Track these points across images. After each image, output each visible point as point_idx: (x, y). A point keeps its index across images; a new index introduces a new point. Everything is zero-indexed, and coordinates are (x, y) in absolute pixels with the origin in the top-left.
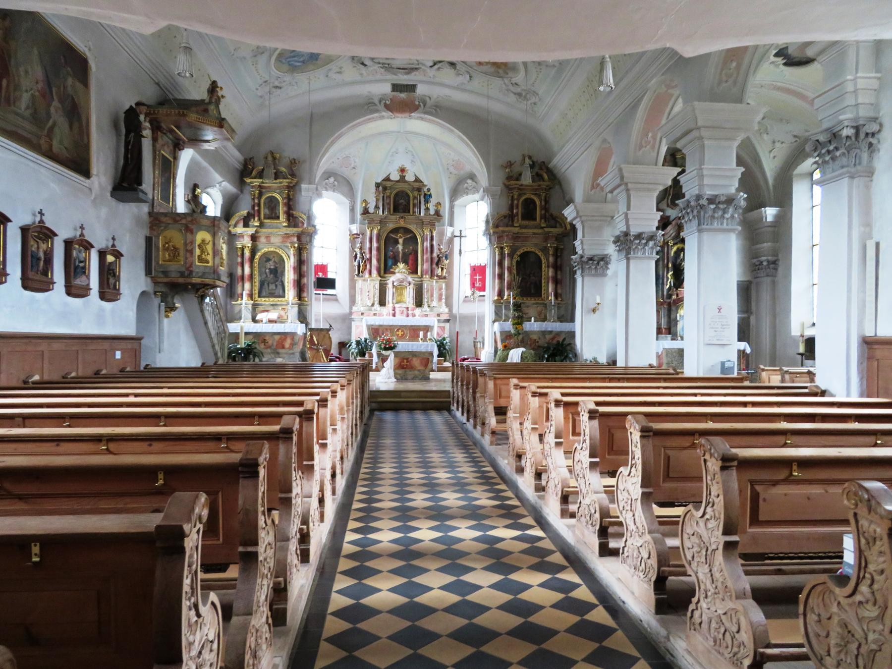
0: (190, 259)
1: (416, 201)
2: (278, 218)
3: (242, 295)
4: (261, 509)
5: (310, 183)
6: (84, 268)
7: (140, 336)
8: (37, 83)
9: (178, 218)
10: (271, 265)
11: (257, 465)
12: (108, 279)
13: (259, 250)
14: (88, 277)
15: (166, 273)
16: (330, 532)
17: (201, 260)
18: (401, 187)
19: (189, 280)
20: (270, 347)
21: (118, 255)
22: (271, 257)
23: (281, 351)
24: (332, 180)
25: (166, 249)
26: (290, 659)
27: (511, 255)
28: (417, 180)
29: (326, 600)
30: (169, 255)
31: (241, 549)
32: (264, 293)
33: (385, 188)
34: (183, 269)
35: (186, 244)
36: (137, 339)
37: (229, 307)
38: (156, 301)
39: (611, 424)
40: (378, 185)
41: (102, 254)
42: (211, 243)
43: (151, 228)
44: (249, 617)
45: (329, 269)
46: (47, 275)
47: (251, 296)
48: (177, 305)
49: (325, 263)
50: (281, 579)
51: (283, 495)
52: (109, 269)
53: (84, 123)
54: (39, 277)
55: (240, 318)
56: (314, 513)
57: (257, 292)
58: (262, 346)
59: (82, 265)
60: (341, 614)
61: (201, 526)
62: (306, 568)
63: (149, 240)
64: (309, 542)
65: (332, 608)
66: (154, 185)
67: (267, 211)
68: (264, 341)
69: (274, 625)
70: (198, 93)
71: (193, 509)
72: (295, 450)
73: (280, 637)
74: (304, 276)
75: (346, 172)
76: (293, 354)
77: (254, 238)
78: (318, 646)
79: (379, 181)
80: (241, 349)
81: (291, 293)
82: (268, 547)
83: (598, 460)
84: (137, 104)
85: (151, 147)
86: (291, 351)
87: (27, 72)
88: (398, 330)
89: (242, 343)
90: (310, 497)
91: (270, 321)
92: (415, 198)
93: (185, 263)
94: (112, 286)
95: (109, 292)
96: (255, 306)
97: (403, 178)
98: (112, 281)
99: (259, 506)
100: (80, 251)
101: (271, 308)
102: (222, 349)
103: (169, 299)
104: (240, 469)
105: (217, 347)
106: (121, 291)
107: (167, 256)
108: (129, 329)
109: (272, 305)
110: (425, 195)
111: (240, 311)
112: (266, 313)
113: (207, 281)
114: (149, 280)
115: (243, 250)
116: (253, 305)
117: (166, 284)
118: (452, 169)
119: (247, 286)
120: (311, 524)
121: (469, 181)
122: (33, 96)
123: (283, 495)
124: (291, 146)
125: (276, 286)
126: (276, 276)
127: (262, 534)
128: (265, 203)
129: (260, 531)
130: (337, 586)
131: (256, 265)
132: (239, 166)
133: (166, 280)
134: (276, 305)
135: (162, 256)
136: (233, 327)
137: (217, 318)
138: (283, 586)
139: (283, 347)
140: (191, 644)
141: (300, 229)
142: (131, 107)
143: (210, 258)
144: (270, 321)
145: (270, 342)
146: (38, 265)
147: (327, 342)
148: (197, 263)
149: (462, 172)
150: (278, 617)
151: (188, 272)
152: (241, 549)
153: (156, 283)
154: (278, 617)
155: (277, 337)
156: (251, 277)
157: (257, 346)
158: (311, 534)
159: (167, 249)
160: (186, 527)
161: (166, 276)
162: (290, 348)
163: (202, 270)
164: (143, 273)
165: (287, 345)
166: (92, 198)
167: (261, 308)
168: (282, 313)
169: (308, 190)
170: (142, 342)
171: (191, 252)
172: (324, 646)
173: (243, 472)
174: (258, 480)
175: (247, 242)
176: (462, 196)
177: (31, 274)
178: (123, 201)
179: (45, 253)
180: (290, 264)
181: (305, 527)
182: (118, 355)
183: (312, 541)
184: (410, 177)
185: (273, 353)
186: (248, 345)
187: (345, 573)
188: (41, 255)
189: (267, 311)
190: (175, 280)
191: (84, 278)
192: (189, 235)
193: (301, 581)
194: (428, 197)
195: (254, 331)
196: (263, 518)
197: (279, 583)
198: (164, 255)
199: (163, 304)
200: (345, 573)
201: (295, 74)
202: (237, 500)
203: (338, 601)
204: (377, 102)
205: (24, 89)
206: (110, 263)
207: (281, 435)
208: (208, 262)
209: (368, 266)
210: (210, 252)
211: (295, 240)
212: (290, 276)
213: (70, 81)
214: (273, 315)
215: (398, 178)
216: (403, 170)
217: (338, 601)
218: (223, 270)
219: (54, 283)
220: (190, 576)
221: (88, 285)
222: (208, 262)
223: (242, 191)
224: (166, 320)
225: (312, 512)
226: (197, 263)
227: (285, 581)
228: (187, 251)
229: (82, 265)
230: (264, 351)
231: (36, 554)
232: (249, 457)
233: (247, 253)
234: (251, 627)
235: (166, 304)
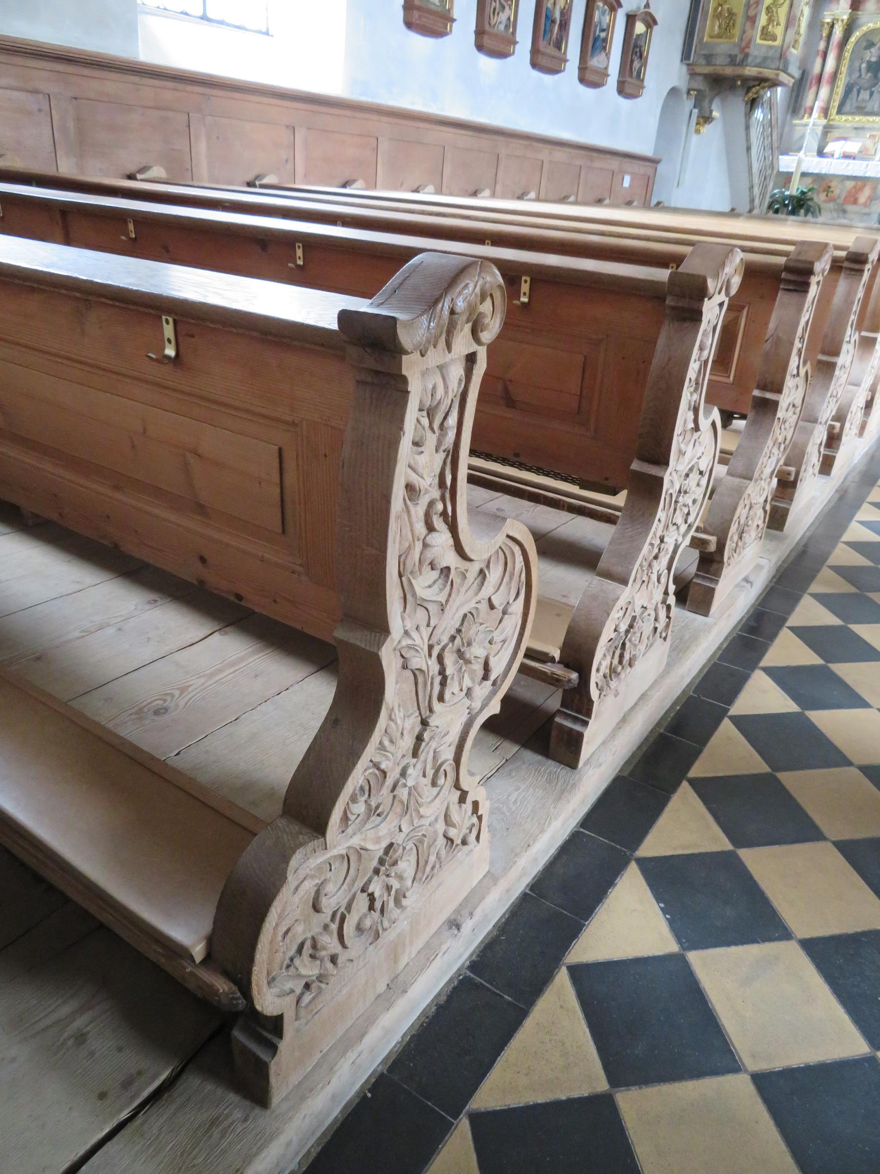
0: (749, 33)
3: (812, 109)
4: (797, 344)
6: (605, 40)
7: (657, 157)
11: (810, 272)
12: (632, 62)
13: (860, 26)
14: (608, 55)
16: (866, 454)
17: (766, 34)
19: (739, 71)
20: (833, 200)
21: (651, 22)
22: (876, 40)
23: (850, 208)
25: (718, 16)
26: (777, 570)
29: (843, 527)
30: (720, 27)
31: (756, 393)
32: (847, 107)
34: (736, 51)
36: (653, 162)
37: (786, 129)
41: (631, 19)
44: (748, 482)
46: (559, 48)
47: (825, 112)
48: (715, 114)
50: (792, 469)
51: (824, 358)
52: (636, 46)
54: (551, 50)
55: (799, 150)
56: (855, 416)
57: (836, 104)
58: (823, 196)
59: (603, 35)
60: (753, 727)
61: (727, 300)
62: (824, 481)
64: (838, 448)
65: (847, 537)
68: (828, 189)
69: (768, 527)
71: (723, 265)
72: (860, 294)
73: (771, 540)
76: (868, 214)
78: (818, 571)
80: (791, 197)
82: (791, 409)
86: (866, 210)
89: (794, 189)
90: (858, 385)
91: (846, 156)
93: (741, 39)
94: (635, 74)
95: (630, 84)
96: (827, 130)
98: (636, 65)
99: (797, 340)
100: (603, 13)
101: (853, 134)
102: (763, 194)
103: (706, 103)
104: (783, 275)
105: (756, 191)
106: (646, 83)
107: (716, 28)
108: (643, 145)
109: (856, 129)
111: (802, 137)
112: (843, 142)
113: (767, 73)
114: (684, 68)
115: (832, 26)
116: (825, 127)
117: (706, 77)
119: (824, 91)
120: (847, 425)
123: (824, 358)
125: (872, 94)
127: (789, 382)
129: (788, 377)
130: (860, 516)
131: (847, 55)
133: (707, 70)
134: (863, 128)
135: (710, 27)
136: (786, 163)
137: (766, 143)
138: (792, 478)
139: (855, 202)
140: (681, 453)
143: (779, 31)
144: (846, 156)
145: (837, 192)
146: (551, 31)
148: (759, 41)
150: (777, 519)
151: (739, 59)
152: (756, 393)
153: (693, 75)
154: (777, 519)
155: (850, 184)
157: (815, 197)
158: (844, 438)
160: (711, 284)
161: (709, 64)
162: (865, 205)
164: (678, 56)
165: (863, 198)
167: (836, 133)
168: (869, 143)
170: (660, 167)
172: (826, 573)
173: (789, 282)
174: (806, 297)
177: (542, 44)
179: (562, 14)
181: (838, 425)
182: (627, 181)
183: (842, 448)
186: (803, 193)
187: (802, 633)
188: (557, 15)
190: (719, 70)
191: (603, 56)
193: (813, 495)
195: (816, 171)
196: (797, 359)
197: (789, 474)
198: (713, 26)
199: (696, 111)
200: (802, 633)
202: (767, 324)
203: (761, 696)
206: (639, 36)
207: (846, 264)
208: (774, 38)
210: (783, 19)
214: (852, 147)
217: (761, 696)
218: (795, 53)
219: (566, 61)
220: (698, 364)
221: (606, 68)
222: (774, 38)
224: (694, 138)
225: (853, 408)
226: (759, 41)
227: (797, 474)
229: (603, 35)
230: (823, 206)
231: (525, 294)
232: (802, 258)
234: (745, 496)
235: (700, 111)
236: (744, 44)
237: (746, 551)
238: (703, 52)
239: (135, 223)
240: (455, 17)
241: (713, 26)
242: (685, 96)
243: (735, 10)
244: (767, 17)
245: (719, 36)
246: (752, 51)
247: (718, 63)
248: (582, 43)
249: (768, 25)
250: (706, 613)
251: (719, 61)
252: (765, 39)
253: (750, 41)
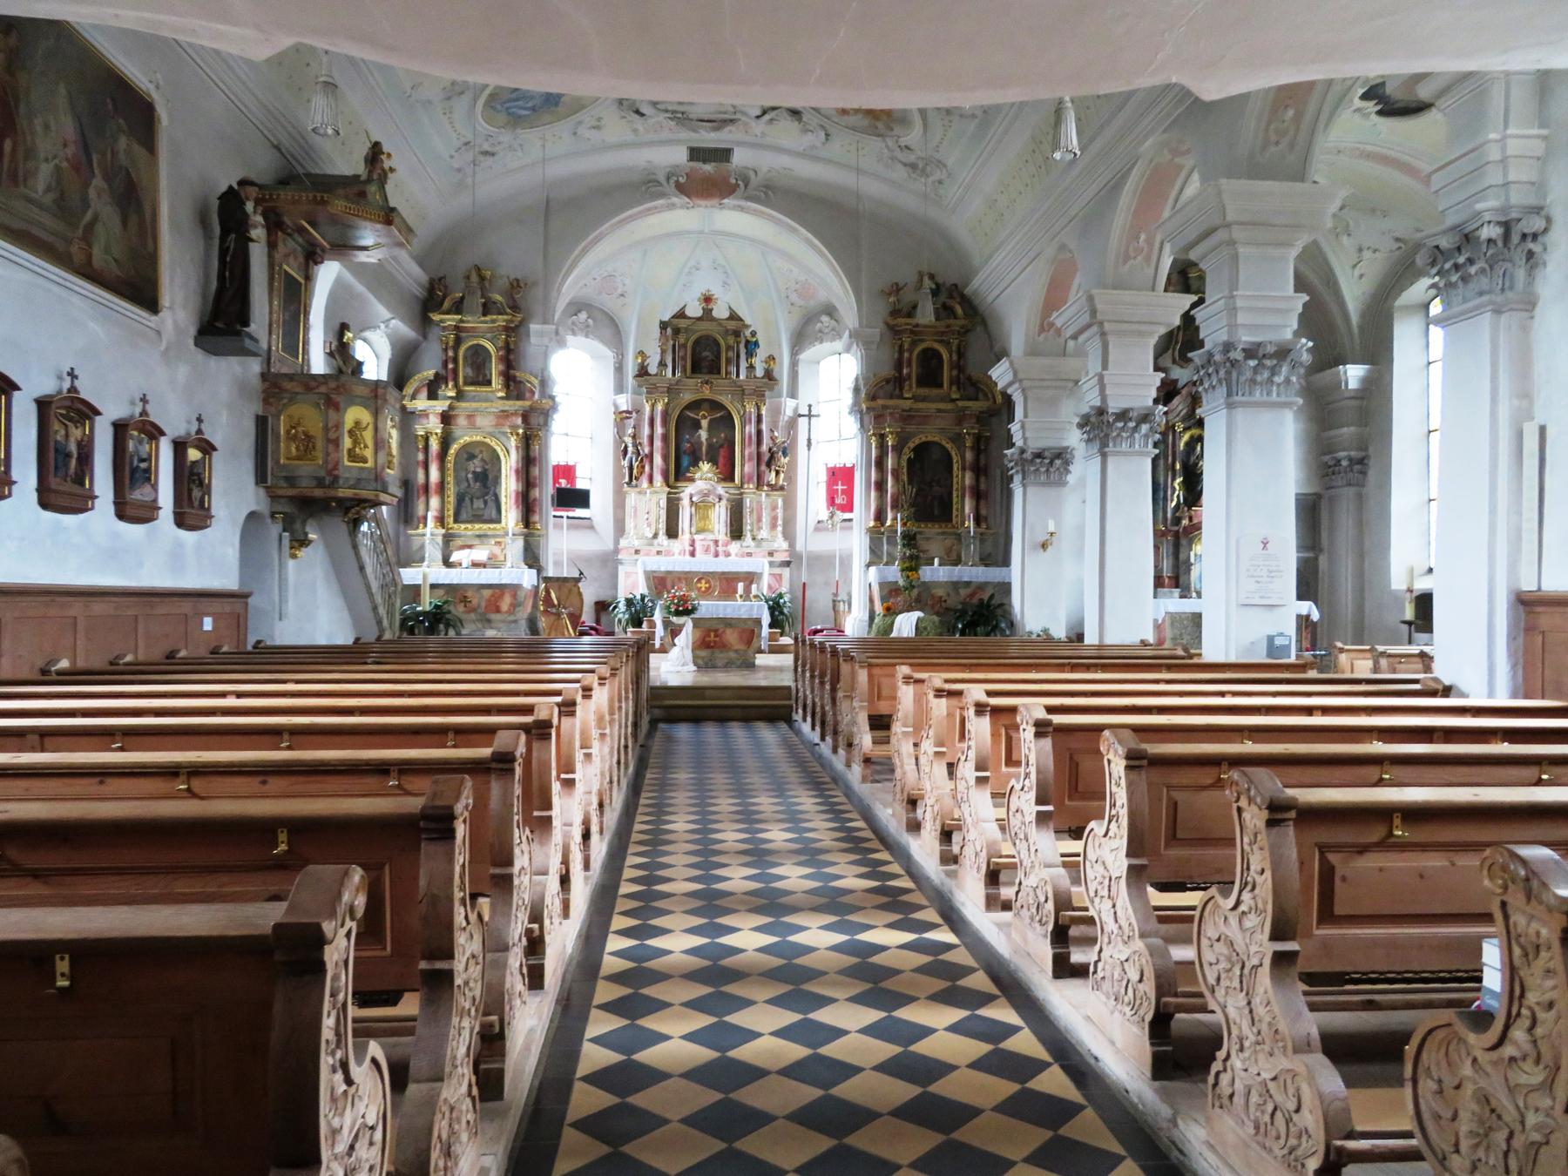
0: (333, 456)
1: (730, 354)
2: (489, 383)
3: (425, 518)
4: (458, 895)
5: (545, 323)
6: (148, 470)
7: (246, 590)
8: (65, 146)
9: (313, 384)
10: (476, 466)
11: (451, 817)
12: (190, 491)
13: (455, 440)
14: (155, 487)
15: (291, 480)
16: (579, 936)
17: (353, 456)
18: (705, 328)
19: (331, 493)
20: (474, 610)
21: (207, 448)
22: (477, 451)
23: (494, 616)
24: (583, 316)
25: (291, 438)
26: (510, 1158)
27: (898, 449)
28: (734, 317)
29: (573, 1055)
31: (423, 965)
32: (464, 516)
33: (677, 331)
34: (322, 473)
35: (326, 429)
36: (241, 596)
37: (402, 539)
38: (275, 529)
39: (1073, 745)
40: (664, 326)
41: (179, 447)
42: (371, 427)
43: (266, 401)
44: (438, 1084)
45: (578, 473)
46: (82, 484)
47: (441, 520)
48: (311, 536)
49: (571, 463)
50: (494, 1018)
51: (498, 871)
52: (192, 474)
53: (148, 216)
54: (69, 487)
55: (422, 560)
56: (553, 902)
57: (451, 513)
58: (461, 608)
59: (143, 465)
60: (599, 1079)
61: (354, 925)
62: (538, 999)
64: (543, 953)
65: (583, 1069)
66: (270, 325)
67: (469, 371)
68: (465, 600)
70: (349, 163)
71: (339, 895)
72: (518, 790)
73: (492, 1120)
74: (534, 486)
75: (609, 303)
76: (515, 621)
77: (446, 418)
78: (559, 1136)
79: (666, 318)
80: (424, 613)
81: (511, 515)
82: (472, 962)
84: (241, 183)
85: (265, 259)
86: (512, 618)
87: (47, 127)
88: (699, 580)
89: (426, 603)
90: (545, 873)
91: (475, 565)
92: (729, 348)
93: (326, 462)
94: (196, 503)
95: (192, 513)
96: (448, 539)
97: (708, 313)
98: (196, 493)
99: (456, 890)
100: (140, 442)
101: (476, 542)
102: (390, 613)
103: (298, 526)
104: (422, 824)
105: (382, 611)
106: (213, 512)
107: (293, 450)
108: (226, 578)
109: (479, 536)
110: (747, 342)
111: (422, 547)
112: (467, 551)
113: (364, 494)
114: (262, 492)
115: (426, 439)
116: (445, 536)
117: (292, 499)
118: (794, 297)
119: (435, 502)
120: (547, 922)
121: (825, 319)
122: (58, 169)
123: (498, 871)
124: (511, 257)
125: (486, 503)
126: (485, 485)
127: (460, 939)
128: (465, 358)
129: (457, 934)
130: (592, 1031)
131: (450, 466)
132: (419, 292)
133: (291, 492)
134: (486, 536)
135: (285, 451)
136: (409, 576)
137: (382, 559)
138: (497, 1029)
139: (498, 610)
140: (335, 1132)
141: (528, 403)
142: (231, 187)
143: (369, 453)
144: (475, 565)
145: (475, 602)
146: (67, 466)
147: (576, 601)
148: (347, 463)
149: (812, 303)
150: (489, 1085)
151: (331, 478)
152: (423, 965)
153: (274, 497)
154: (489, 1085)
155: (487, 593)
156: (442, 486)
157: (451, 608)
158: (547, 939)
159: (293, 438)
160: (328, 927)
161: (293, 486)
162: (510, 612)
163: (355, 474)
164: (251, 479)
165: (505, 606)
166: (162, 348)
168: (497, 550)
169: (541, 334)
170: (250, 600)
171: (336, 443)
172: (569, 1135)
173: (426, 830)
174: (453, 844)
175: (434, 425)
176: (812, 344)
177: (54, 482)
178: (216, 354)
179: (79, 444)
180: (510, 463)
181: (535, 926)
182: (208, 624)
183: (549, 951)
184: (720, 312)
185: (480, 620)
186: (437, 607)
187: (606, 1007)
188: (73, 448)
189: (470, 547)
190: (308, 493)
191: (147, 489)
192: (332, 413)
193: (529, 1021)
194: (752, 347)
195: (447, 582)
196: (462, 910)
197: (491, 1025)
198: (288, 448)
199: (286, 534)
200: (606, 1007)
201: (519, 131)
202: (416, 878)
204: (662, 179)
206: (194, 463)
207: (494, 765)
208: (365, 461)
209: (647, 468)
210: (370, 442)
211: (519, 421)
212: (509, 485)
213: (123, 142)
214: (480, 554)
215: (699, 313)
216: (708, 299)
217: (594, 1057)
218: (392, 474)
219: (94, 497)
221: (155, 500)
222: (365, 461)
223: (425, 337)
224: (291, 563)
225: (548, 901)
226: (347, 463)
227: (502, 1021)
228: (329, 441)
229: (143, 465)
230: (463, 617)
231: (63, 975)
232: (438, 803)
233: (434, 445)
234: (441, 1103)
235: (292, 534)
237: (461, 1163)
242: (269, 521)
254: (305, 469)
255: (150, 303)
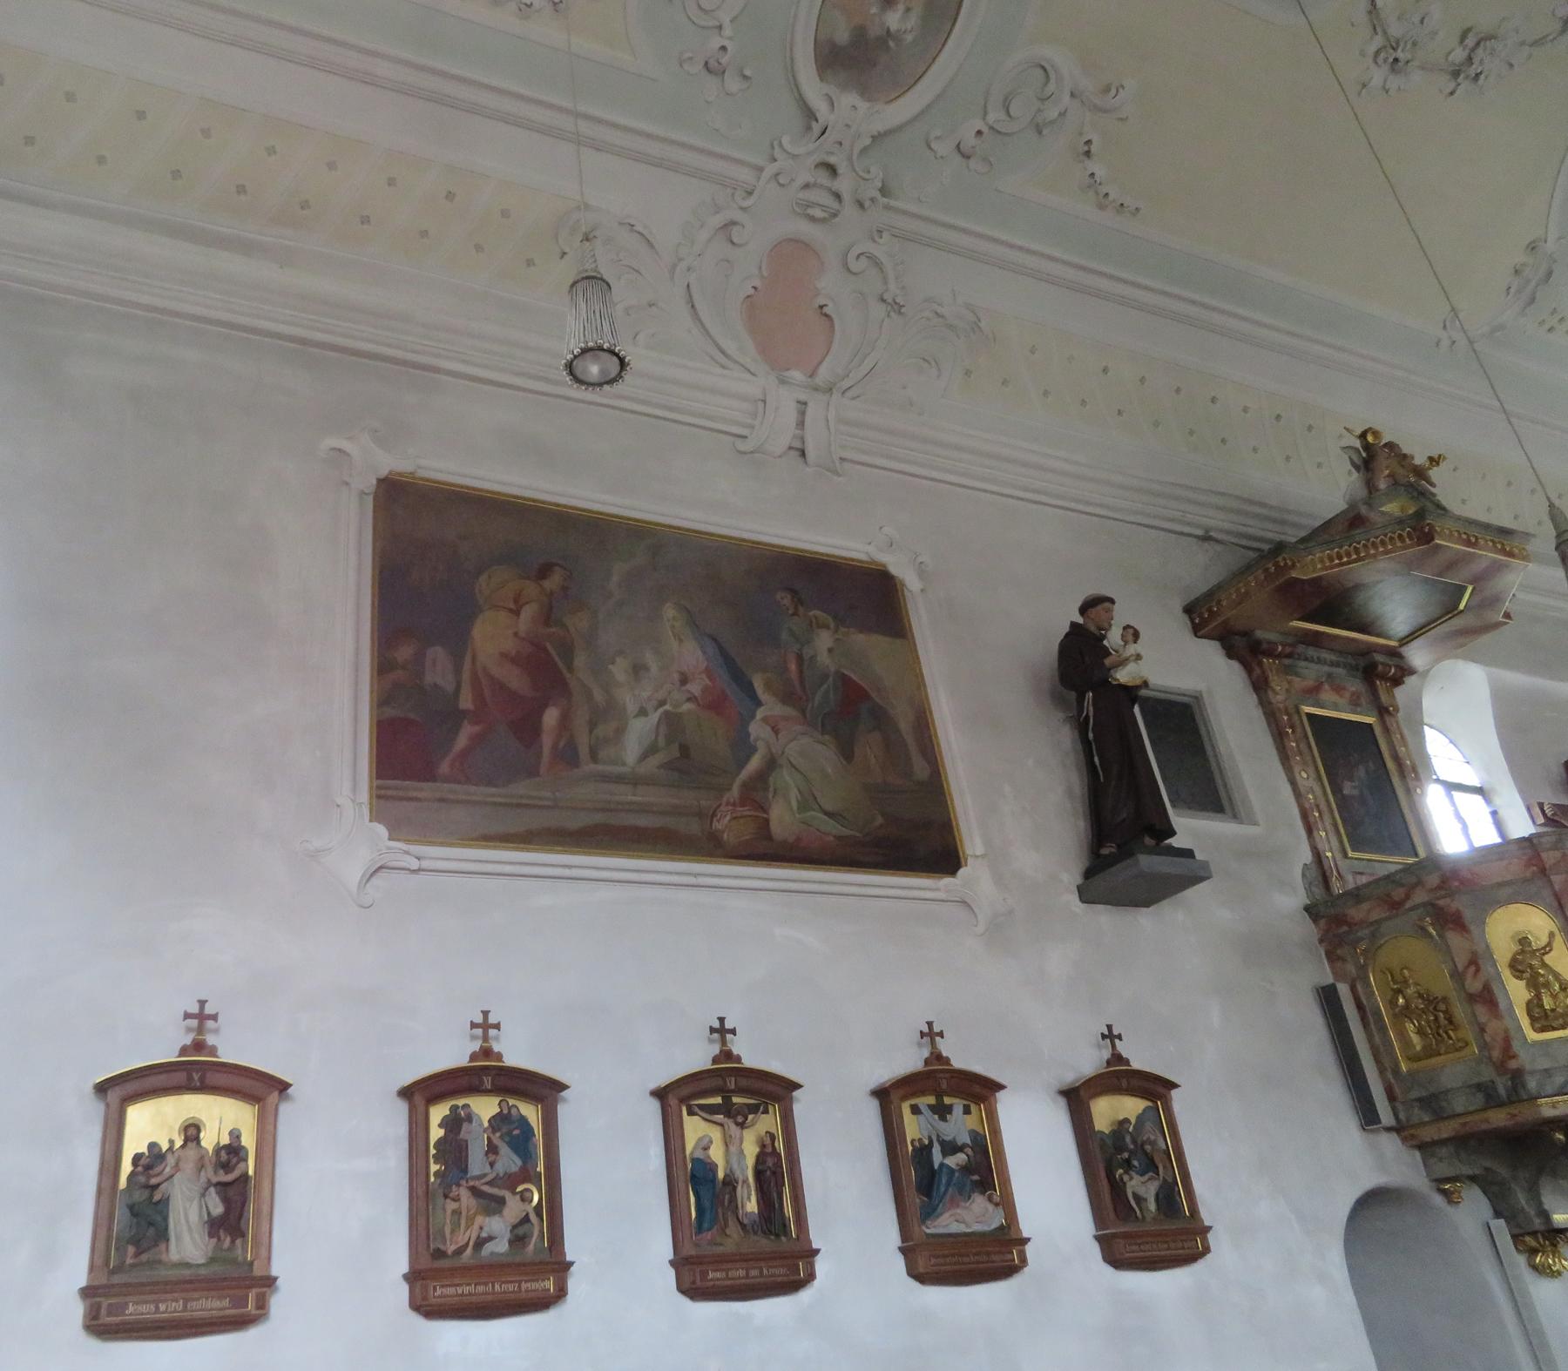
0: (1493, 1027)
8: (684, 681)
9: (1398, 894)
15: (1433, 1104)
21: (1155, 1088)
30: (1420, 1032)
32: (706, 1225)
34: (1487, 1074)
35: (1458, 976)
38: (1471, 1214)
43: (1332, 957)
53: (905, 726)
63: (1328, 998)
66: (1305, 816)
70: (1328, 488)
83: (1470, 589)
84: (1084, 609)
85: (1257, 714)
87: (638, 670)
93: (1484, 1046)
106: (1207, 1218)
107: (1415, 1039)
122: (672, 722)
133: (1447, 1130)
142: (1074, 625)
159: (1406, 1012)
161: (1440, 1117)
164: (1348, 1122)
166: (981, 929)
171: (1488, 998)
178: (1147, 904)
192: (1454, 939)
198: (1402, 1035)
205: (632, 707)
213: (824, 641)
226: (1532, 1036)
228: (1472, 998)
236: (1496, 1054)
238: (1415, 1094)
239: (929, 1213)
240: (1207, 1223)
241: (1402, 1035)
243: (1438, 991)
244: (1522, 984)
245: (1429, 1052)
246: (1524, 1059)
247: (1459, 1109)
248: (899, 1215)
249: (1538, 996)
250: (397, 497)
251: (1459, 1104)
252: (1543, 1030)
253: (1507, 1041)
254: (1453, 1072)
255: (940, 856)
